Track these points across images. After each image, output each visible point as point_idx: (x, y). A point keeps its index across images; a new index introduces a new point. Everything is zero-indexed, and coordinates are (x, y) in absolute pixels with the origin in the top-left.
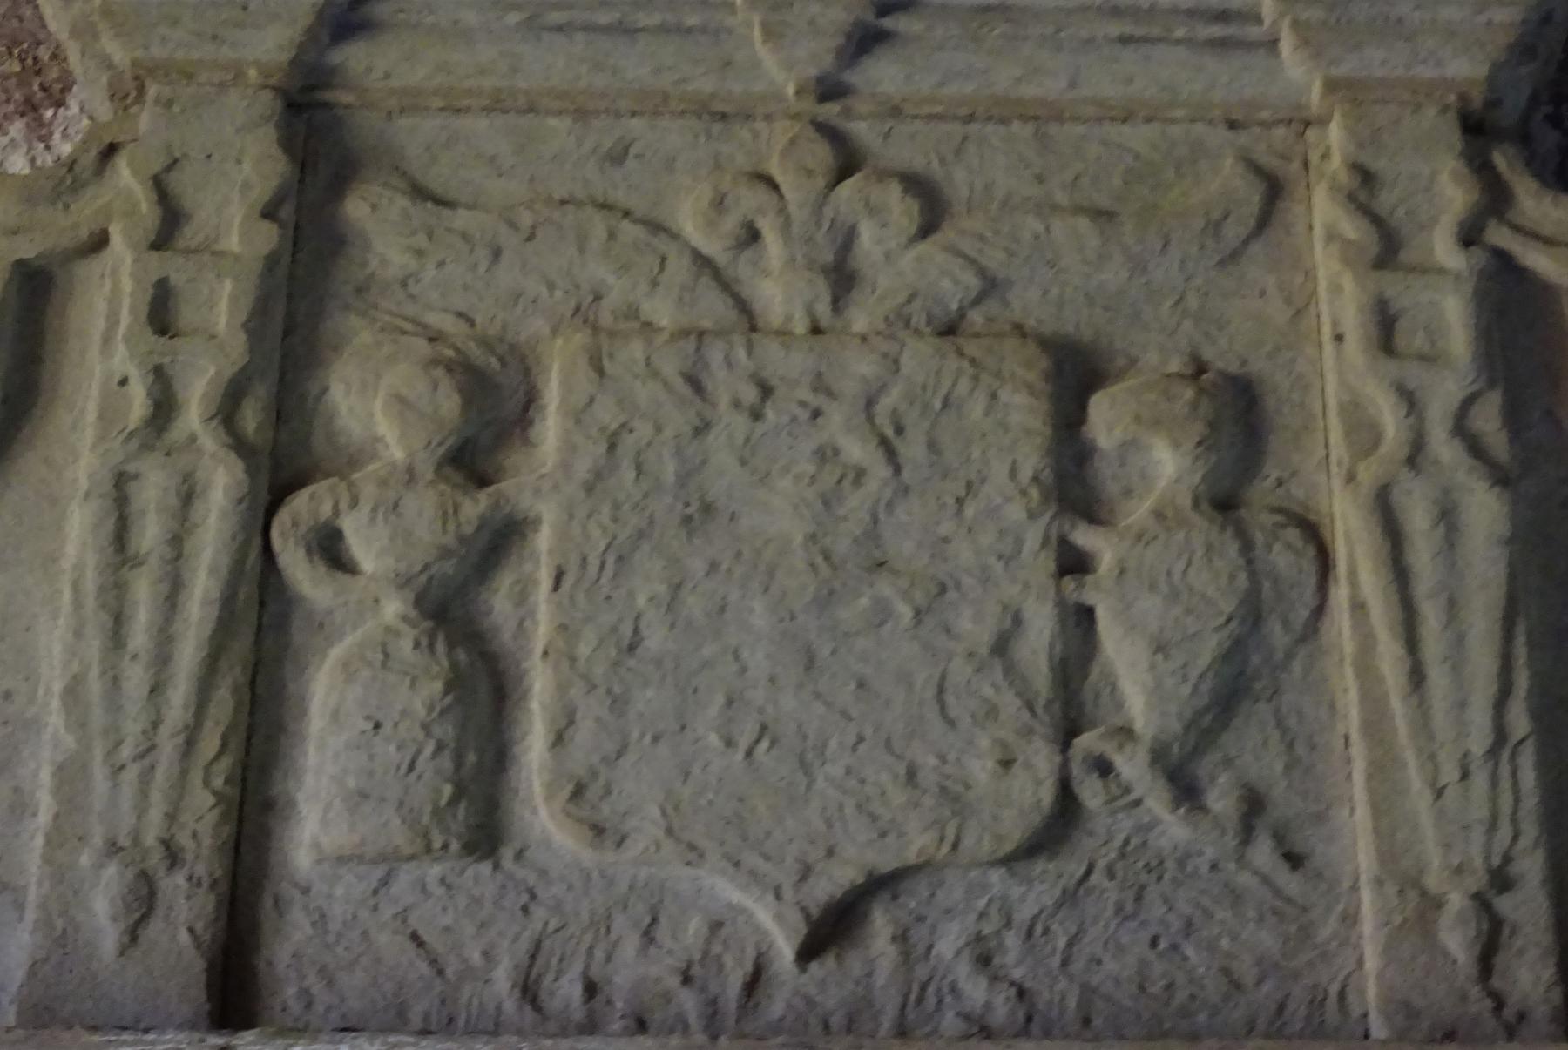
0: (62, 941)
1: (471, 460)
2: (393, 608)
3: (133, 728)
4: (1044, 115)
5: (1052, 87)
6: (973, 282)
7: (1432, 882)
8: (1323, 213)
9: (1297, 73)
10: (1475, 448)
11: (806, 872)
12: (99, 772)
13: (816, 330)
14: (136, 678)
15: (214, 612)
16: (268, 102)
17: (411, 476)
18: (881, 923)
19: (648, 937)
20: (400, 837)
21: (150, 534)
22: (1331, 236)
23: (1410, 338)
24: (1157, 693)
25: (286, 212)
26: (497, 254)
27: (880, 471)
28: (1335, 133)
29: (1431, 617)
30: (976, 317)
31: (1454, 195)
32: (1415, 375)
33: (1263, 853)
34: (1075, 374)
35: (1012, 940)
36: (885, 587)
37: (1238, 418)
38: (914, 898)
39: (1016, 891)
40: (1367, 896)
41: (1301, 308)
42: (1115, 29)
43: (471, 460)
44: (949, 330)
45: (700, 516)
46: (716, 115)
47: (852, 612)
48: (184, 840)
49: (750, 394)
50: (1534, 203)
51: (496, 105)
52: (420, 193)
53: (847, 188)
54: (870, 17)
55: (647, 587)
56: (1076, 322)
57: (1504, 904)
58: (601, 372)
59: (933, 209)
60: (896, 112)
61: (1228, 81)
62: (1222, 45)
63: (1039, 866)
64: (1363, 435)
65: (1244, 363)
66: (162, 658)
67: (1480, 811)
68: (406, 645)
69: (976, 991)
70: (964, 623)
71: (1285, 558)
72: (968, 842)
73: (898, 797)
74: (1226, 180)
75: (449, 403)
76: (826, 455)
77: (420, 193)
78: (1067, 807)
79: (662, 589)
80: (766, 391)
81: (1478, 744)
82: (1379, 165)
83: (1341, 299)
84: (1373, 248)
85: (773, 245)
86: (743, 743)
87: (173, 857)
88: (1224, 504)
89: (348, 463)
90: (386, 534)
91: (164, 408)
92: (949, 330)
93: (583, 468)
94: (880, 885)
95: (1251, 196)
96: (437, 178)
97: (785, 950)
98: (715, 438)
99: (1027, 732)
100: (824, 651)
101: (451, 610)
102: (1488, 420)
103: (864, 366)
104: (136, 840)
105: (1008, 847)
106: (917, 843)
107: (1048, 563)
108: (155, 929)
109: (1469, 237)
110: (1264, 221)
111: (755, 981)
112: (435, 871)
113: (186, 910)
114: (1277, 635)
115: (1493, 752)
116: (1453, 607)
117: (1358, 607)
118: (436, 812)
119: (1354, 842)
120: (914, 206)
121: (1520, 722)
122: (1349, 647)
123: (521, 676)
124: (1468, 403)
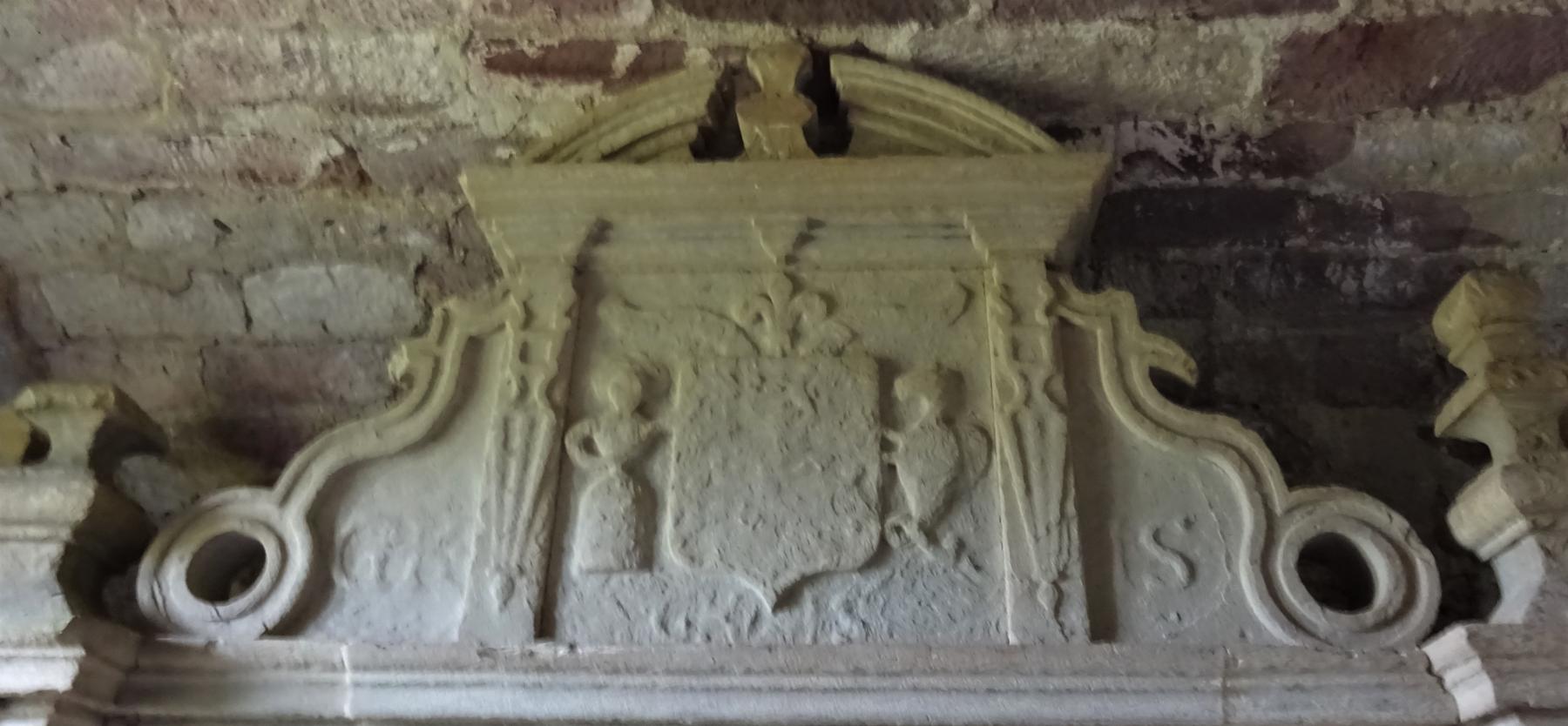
1: (643, 410)
2: (613, 470)
3: (508, 520)
4: (876, 268)
6: (847, 334)
7: (1036, 574)
8: (990, 304)
10: (1051, 396)
11: (776, 575)
12: (494, 538)
13: (784, 355)
14: (509, 499)
15: (541, 474)
17: (621, 417)
18: (808, 596)
19: (713, 602)
20: (612, 561)
21: (517, 442)
23: (1026, 353)
24: (921, 499)
25: (574, 314)
26: (658, 328)
28: (995, 272)
29: (1034, 466)
30: (849, 349)
31: (1043, 294)
33: (965, 565)
34: (887, 371)
35: (861, 603)
37: (955, 389)
39: (863, 582)
40: (1007, 583)
44: (839, 353)
45: (736, 430)
48: (527, 565)
49: (757, 381)
50: (1077, 297)
51: (660, 269)
52: (628, 304)
53: (798, 300)
54: (806, 230)
57: (1064, 586)
58: (696, 372)
59: (831, 304)
60: (818, 268)
64: (1005, 391)
65: (390, 279)
66: (519, 493)
67: (1054, 547)
68: (618, 485)
69: (845, 623)
70: (843, 473)
71: (974, 443)
72: (843, 562)
73: (813, 542)
74: (950, 291)
75: (637, 387)
76: (787, 405)
77: (628, 304)
78: (884, 546)
79: (720, 461)
80: (763, 379)
83: (996, 338)
85: (767, 321)
86: (751, 523)
87: (521, 570)
88: (948, 420)
91: (524, 390)
93: (689, 412)
94: (807, 580)
95: (962, 297)
97: (767, 607)
99: (867, 518)
100: (785, 485)
102: (1058, 386)
103: (802, 369)
104: (507, 564)
105: (859, 564)
106: (822, 563)
107: (876, 447)
108: (514, 601)
109: (1049, 311)
110: (966, 308)
111: (756, 619)
112: (626, 577)
115: (1060, 523)
116: (1043, 462)
117: (1004, 463)
118: (628, 553)
120: (824, 307)
121: (1071, 508)
122: (1000, 480)
123: (663, 496)
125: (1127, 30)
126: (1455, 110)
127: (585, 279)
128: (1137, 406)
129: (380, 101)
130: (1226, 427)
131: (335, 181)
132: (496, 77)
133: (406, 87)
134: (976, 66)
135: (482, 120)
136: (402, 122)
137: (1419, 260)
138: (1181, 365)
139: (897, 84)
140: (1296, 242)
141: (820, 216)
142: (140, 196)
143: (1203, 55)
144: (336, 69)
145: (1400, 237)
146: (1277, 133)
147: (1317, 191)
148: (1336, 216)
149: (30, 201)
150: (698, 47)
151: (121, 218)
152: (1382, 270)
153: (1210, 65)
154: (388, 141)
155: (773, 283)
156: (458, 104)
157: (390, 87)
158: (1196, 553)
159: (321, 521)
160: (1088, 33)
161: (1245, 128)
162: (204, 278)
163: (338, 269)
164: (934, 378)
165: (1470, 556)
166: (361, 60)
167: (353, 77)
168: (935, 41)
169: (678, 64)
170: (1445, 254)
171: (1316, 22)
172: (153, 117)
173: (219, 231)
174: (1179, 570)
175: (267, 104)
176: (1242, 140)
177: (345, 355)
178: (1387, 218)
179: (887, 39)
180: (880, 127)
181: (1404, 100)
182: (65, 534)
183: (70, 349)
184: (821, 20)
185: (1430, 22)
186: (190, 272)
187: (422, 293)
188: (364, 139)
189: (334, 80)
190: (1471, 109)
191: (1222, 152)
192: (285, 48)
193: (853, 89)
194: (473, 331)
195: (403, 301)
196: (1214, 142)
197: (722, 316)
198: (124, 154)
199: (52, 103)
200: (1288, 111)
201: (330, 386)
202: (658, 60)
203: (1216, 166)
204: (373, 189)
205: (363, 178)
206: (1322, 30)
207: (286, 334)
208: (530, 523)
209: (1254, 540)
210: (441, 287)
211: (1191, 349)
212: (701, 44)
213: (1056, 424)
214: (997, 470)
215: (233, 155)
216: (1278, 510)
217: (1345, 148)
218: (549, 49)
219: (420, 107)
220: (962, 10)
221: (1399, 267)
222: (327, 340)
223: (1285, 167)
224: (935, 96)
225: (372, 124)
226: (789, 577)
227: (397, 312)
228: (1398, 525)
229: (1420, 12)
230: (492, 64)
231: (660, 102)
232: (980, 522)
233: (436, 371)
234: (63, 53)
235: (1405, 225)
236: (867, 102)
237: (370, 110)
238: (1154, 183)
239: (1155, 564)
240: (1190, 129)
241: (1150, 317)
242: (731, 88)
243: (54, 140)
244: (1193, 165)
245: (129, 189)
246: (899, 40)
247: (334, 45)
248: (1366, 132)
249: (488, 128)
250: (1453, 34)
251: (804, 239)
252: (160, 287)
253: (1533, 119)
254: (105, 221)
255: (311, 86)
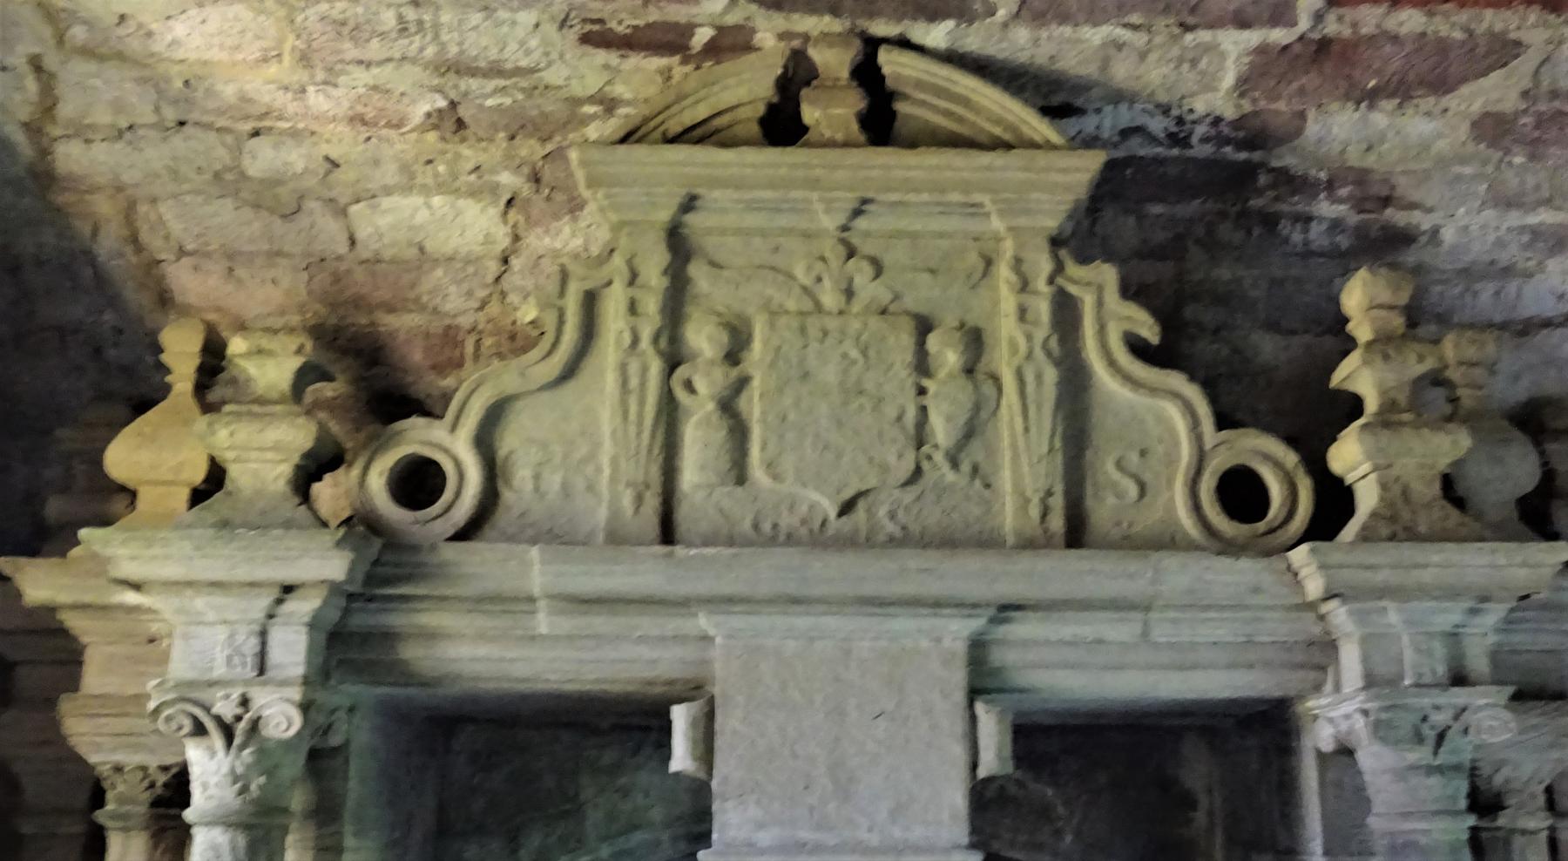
0: (615, 513)
1: (733, 357)
2: (711, 406)
4: (914, 236)
5: (918, 227)
7: (1029, 493)
8: (1004, 272)
9: (997, 224)
10: (1049, 354)
11: (839, 492)
14: (632, 429)
16: (663, 234)
18: (861, 505)
20: (714, 479)
21: (634, 382)
22: (1008, 282)
23: (1030, 316)
27: (861, 361)
31: (1045, 265)
32: (1028, 327)
33: (978, 483)
34: (924, 326)
36: (863, 400)
37: (975, 341)
38: (871, 498)
41: (996, 303)
42: (940, 209)
43: (733, 357)
44: (884, 312)
45: (805, 376)
46: (807, 235)
47: (854, 405)
50: (1073, 269)
52: (714, 264)
55: (788, 401)
56: (922, 309)
57: (1051, 501)
59: (878, 268)
61: (975, 226)
62: (973, 215)
63: (908, 488)
64: (1014, 349)
65: (482, 211)
66: (640, 423)
71: (988, 389)
74: (973, 259)
75: (725, 338)
76: (845, 356)
77: (714, 264)
78: (918, 472)
81: (1045, 449)
82: (1023, 255)
83: (1008, 302)
84: (1019, 286)
85: (827, 283)
88: (969, 371)
89: (693, 357)
90: (707, 382)
91: (635, 341)
92: (884, 312)
93: (768, 359)
95: (981, 266)
96: (720, 257)
97: (832, 513)
98: (810, 349)
101: (728, 406)
102: (1054, 343)
103: (855, 325)
106: (872, 481)
111: (824, 523)
113: (652, 503)
114: (984, 415)
117: (1010, 407)
119: (1005, 480)
121: (1058, 444)
124: (1047, 340)
125: (1125, 35)
126: (1389, 105)
127: (678, 244)
128: (1112, 363)
129: (483, 64)
130: (1176, 380)
131: (436, 127)
132: (589, 49)
133: (507, 54)
134: (1001, 56)
135: (574, 82)
136: (502, 82)
137: (1354, 219)
138: (1149, 331)
139: (935, 75)
140: (1256, 203)
141: (870, 195)
142: (256, 133)
143: (1190, 55)
144: (445, 37)
145: (1341, 201)
146: (1243, 117)
147: (1275, 163)
148: (1291, 183)
149: (152, 134)
150: (766, 30)
151: (237, 150)
152: (1324, 226)
153: (1194, 63)
154: (487, 97)
155: (834, 253)
156: (553, 68)
157: (493, 54)
158: (1147, 477)
159: (485, 442)
160: (1095, 35)
161: (1218, 113)
162: (311, 205)
163: (437, 200)
164: (958, 334)
165: (1338, 481)
166: (476, 36)
167: (460, 44)
168: (968, 36)
169: (748, 47)
170: (1373, 216)
171: (1279, 36)
172: (273, 70)
173: (329, 166)
174: (1132, 490)
175: (381, 63)
176: (1217, 121)
177: (439, 272)
178: (1330, 185)
179: (928, 33)
180: (1031, 656)
181: (1347, 97)
182: (296, 459)
183: (184, 260)
184: (872, 15)
185: (1371, 39)
186: (302, 197)
187: (511, 223)
188: (466, 94)
189: (443, 46)
190: (1400, 106)
191: (1201, 130)
192: (401, 19)
193: (898, 77)
194: (588, 285)
195: (493, 230)
196: (1194, 122)
197: (790, 276)
198: (245, 99)
199: (180, 54)
200: (1254, 101)
201: (425, 299)
202: (731, 43)
203: (1194, 140)
204: (468, 132)
205: (460, 124)
206: (1285, 42)
207: (388, 254)
208: (650, 451)
209: (1188, 468)
210: (528, 219)
211: (1156, 312)
212: (769, 31)
213: (1051, 375)
214: (1004, 410)
215: (346, 104)
216: (1208, 446)
217: (1299, 132)
218: (636, 28)
219: (518, 72)
220: (992, 12)
221: (1336, 225)
222: (424, 258)
223: (1250, 144)
224: (966, 87)
225: (474, 84)
226: (848, 494)
227: (488, 240)
228: (1290, 458)
229: (1364, 31)
230: (586, 39)
231: (732, 81)
232: (991, 452)
233: (561, 321)
234: (193, 12)
235: (1344, 192)
236: (908, 90)
237: (473, 72)
238: (1142, 153)
239: (1114, 486)
240: (1175, 112)
241: (1130, 291)
242: (797, 77)
243: (179, 84)
244: (1175, 139)
245: (248, 126)
246: (937, 35)
247: (445, 17)
248: (1316, 121)
249: (578, 90)
250: (1388, 48)
251: (857, 213)
252: (272, 211)
253: (1450, 113)
254: (221, 152)
255: (422, 49)
